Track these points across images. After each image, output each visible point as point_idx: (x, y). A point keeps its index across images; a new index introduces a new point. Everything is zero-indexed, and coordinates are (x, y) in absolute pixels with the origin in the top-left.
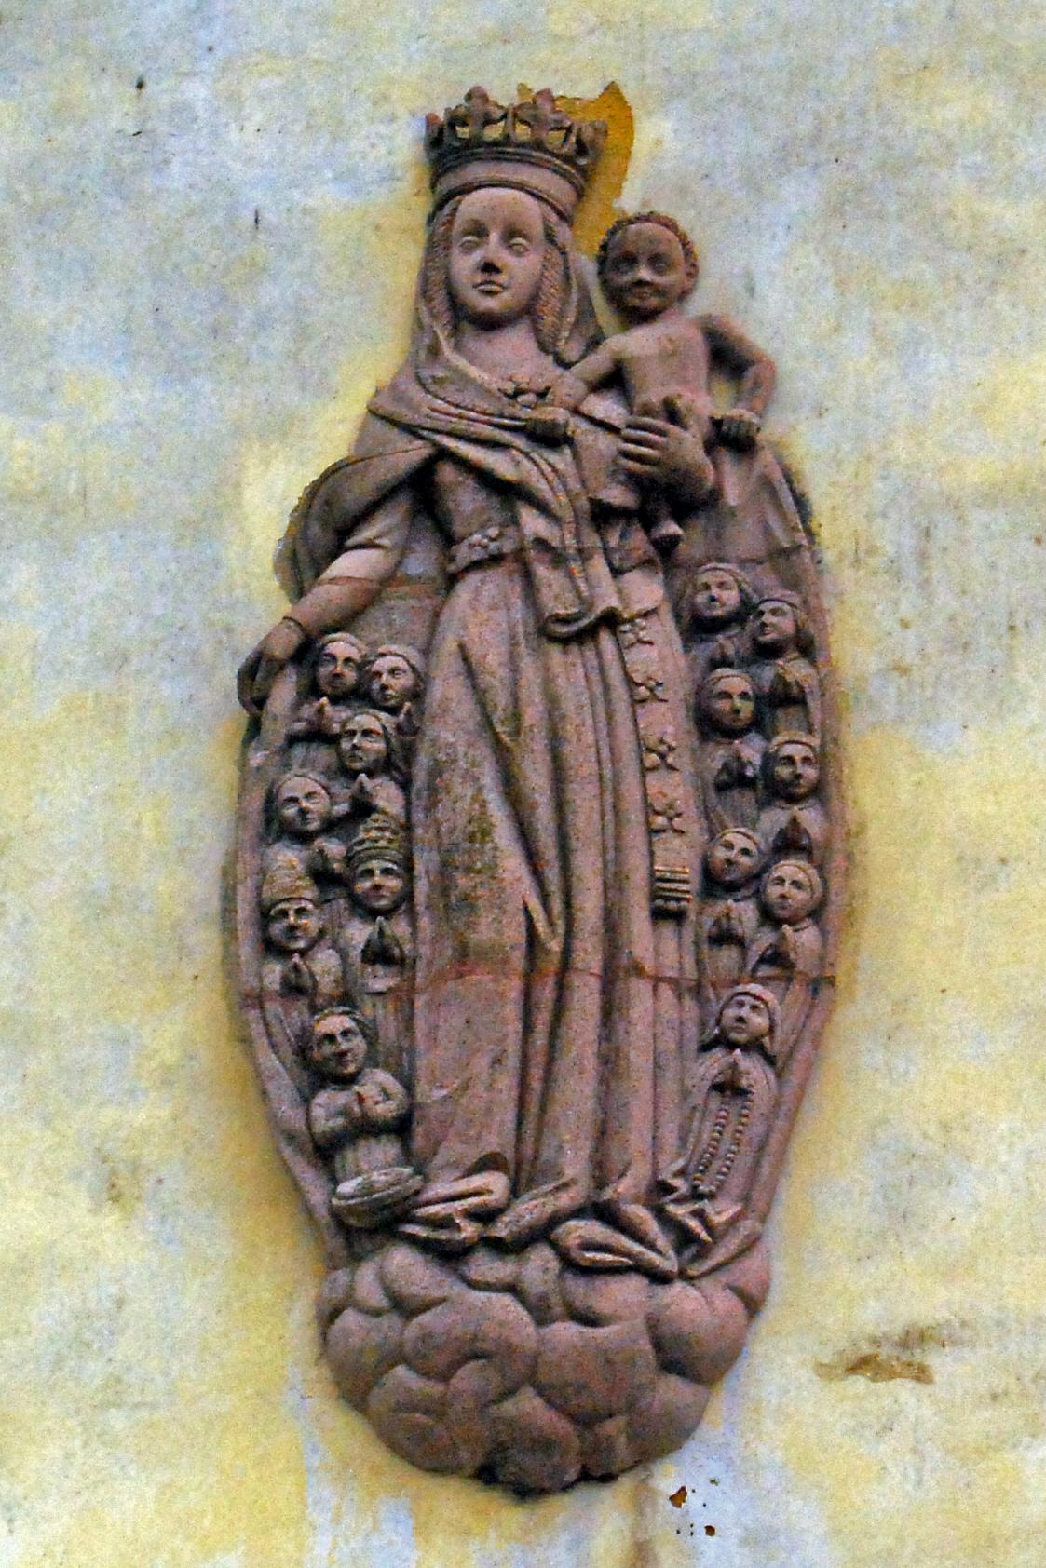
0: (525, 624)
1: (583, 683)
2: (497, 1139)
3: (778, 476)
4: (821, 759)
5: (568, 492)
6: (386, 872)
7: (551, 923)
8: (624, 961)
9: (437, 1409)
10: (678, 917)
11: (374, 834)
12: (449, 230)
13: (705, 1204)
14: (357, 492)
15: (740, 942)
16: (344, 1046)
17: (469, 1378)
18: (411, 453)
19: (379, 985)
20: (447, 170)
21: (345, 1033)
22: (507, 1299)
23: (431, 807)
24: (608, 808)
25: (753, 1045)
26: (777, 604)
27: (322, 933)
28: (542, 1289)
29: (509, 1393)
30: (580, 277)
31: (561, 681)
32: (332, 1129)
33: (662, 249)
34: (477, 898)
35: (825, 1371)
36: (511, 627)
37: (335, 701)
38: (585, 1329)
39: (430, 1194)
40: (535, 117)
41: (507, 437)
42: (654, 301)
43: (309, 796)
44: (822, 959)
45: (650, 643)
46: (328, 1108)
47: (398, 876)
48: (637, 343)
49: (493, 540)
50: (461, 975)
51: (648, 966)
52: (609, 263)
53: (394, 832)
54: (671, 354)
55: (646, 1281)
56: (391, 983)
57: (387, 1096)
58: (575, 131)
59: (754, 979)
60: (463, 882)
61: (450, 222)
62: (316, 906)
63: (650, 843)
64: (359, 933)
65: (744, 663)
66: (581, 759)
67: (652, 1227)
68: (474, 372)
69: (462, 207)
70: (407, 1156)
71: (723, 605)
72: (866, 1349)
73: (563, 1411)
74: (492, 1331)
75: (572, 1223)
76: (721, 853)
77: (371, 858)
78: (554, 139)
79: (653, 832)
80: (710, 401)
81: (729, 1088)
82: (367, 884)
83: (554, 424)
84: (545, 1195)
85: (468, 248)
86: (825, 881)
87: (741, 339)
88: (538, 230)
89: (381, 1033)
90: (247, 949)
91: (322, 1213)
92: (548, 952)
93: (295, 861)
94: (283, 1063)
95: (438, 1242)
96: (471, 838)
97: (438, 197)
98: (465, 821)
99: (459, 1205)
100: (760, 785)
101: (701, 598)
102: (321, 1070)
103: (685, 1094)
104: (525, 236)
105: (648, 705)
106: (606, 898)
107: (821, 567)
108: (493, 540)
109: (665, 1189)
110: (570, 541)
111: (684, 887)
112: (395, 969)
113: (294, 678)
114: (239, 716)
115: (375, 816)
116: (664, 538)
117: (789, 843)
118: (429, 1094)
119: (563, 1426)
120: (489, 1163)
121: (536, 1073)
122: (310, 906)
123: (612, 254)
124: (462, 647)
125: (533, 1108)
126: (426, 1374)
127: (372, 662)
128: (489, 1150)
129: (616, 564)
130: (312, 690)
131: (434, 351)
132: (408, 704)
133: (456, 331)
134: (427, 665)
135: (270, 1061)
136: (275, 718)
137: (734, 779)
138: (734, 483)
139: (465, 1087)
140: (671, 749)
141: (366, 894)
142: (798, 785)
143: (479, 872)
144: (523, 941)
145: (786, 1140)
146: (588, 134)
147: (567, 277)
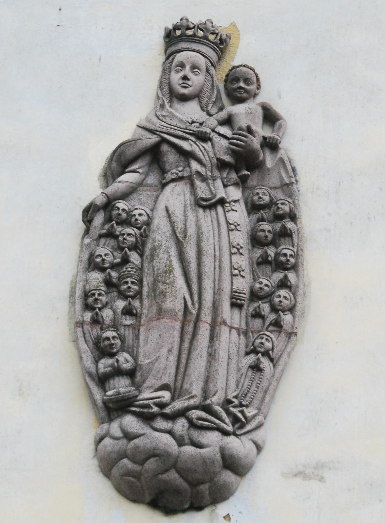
0: (190, 201)
1: (211, 222)
2: (168, 379)
3: (286, 159)
4: (296, 256)
5: (209, 157)
6: (133, 283)
7: (193, 304)
8: (219, 320)
9: (137, 476)
10: (240, 307)
11: (129, 269)
12: (171, 65)
13: (244, 409)
14: (131, 152)
15: (263, 317)
16: (113, 342)
17: (151, 464)
18: (153, 139)
19: (128, 322)
20: (171, 46)
21: (114, 337)
22: (168, 436)
23: (152, 260)
24: (217, 267)
25: (266, 354)
26: (283, 201)
27: (107, 304)
28: (181, 433)
29: (166, 471)
30: (217, 87)
31: (202, 221)
32: (106, 371)
33: (249, 76)
34: (166, 293)
35: (284, 475)
36: (185, 201)
37: (118, 224)
38: (195, 448)
39: (140, 397)
40: (205, 28)
41: (188, 136)
42: (245, 95)
43: (106, 255)
44: (292, 326)
45: (236, 211)
46: (105, 365)
47: (137, 285)
48: (239, 109)
49: (180, 171)
50: (158, 319)
51: (228, 322)
52: (229, 80)
53: (137, 270)
54: (249, 114)
55: (220, 434)
56: (132, 322)
57: (127, 362)
58: (219, 35)
59: (267, 330)
60: (162, 287)
61: (172, 62)
62: (106, 294)
63: (232, 279)
64: (121, 304)
65: (270, 222)
66: (208, 247)
67: (224, 415)
68: (177, 114)
69: (176, 58)
70: (133, 384)
71: (263, 200)
72: (301, 468)
73: (186, 480)
74: (161, 446)
75: (194, 411)
76: (257, 285)
77: (127, 277)
78: (211, 37)
79: (233, 275)
80: (262, 131)
81: (256, 368)
82: (125, 287)
83: (206, 133)
84: (185, 400)
85: (177, 72)
86: (295, 299)
87: (275, 112)
88: (204, 68)
89: (127, 340)
90: (79, 306)
91: (99, 402)
92: (191, 313)
93: (99, 278)
94: (89, 348)
95: (144, 413)
96: (166, 272)
97: (167, 55)
98: (164, 265)
99: (152, 401)
100: (273, 264)
101: (256, 198)
102: (102, 350)
103: (239, 370)
104: (199, 69)
105: (234, 232)
106: (214, 298)
107: (299, 192)
108: (180, 171)
109: (229, 402)
110: (209, 173)
111: (243, 295)
112: (134, 318)
113: (103, 215)
114: (82, 227)
115: (129, 264)
116: (243, 175)
117: (284, 284)
118: (143, 361)
119: (185, 485)
120: (165, 387)
121: (184, 356)
122: (103, 293)
123: (230, 78)
124: (166, 208)
125: (182, 369)
126: (135, 462)
127: (132, 211)
128: (164, 382)
129: (225, 183)
130: (108, 220)
131: (162, 106)
132: (145, 226)
133: (171, 101)
134: (153, 214)
135: (84, 346)
136: (95, 228)
137: (264, 261)
138: (269, 161)
139: (157, 360)
140: (242, 248)
141: (125, 290)
142: (288, 264)
143: (168, 284)
144: (183, 310)
145: (275, 390)
146: (224, 37)
147: (213, 86)
